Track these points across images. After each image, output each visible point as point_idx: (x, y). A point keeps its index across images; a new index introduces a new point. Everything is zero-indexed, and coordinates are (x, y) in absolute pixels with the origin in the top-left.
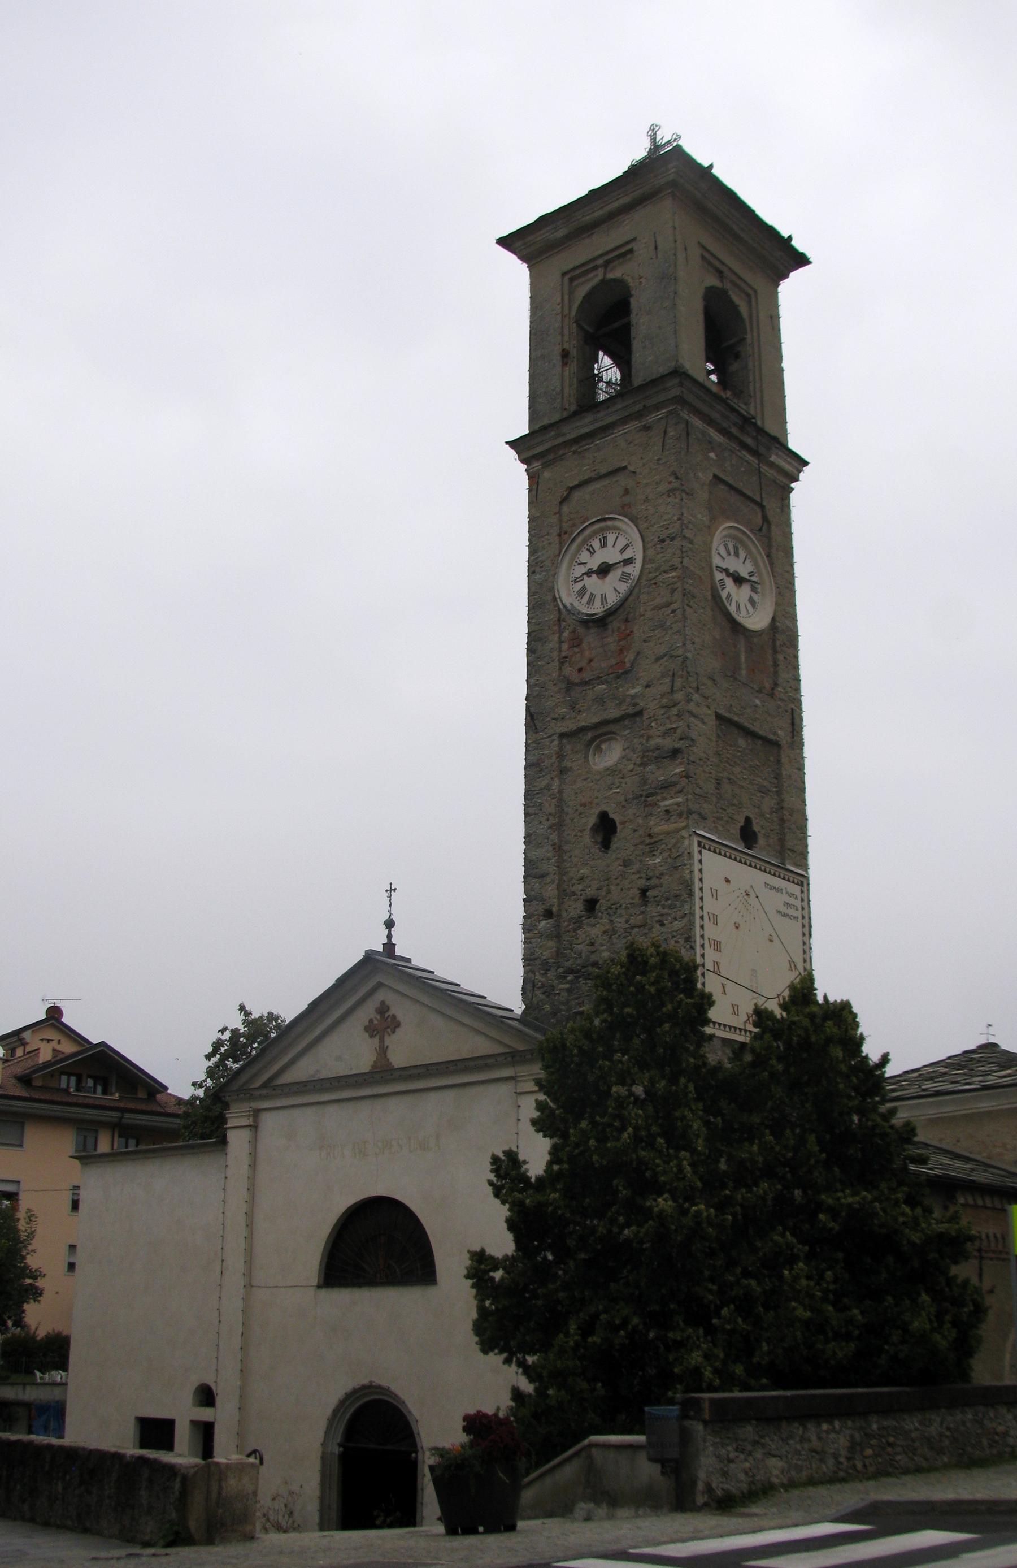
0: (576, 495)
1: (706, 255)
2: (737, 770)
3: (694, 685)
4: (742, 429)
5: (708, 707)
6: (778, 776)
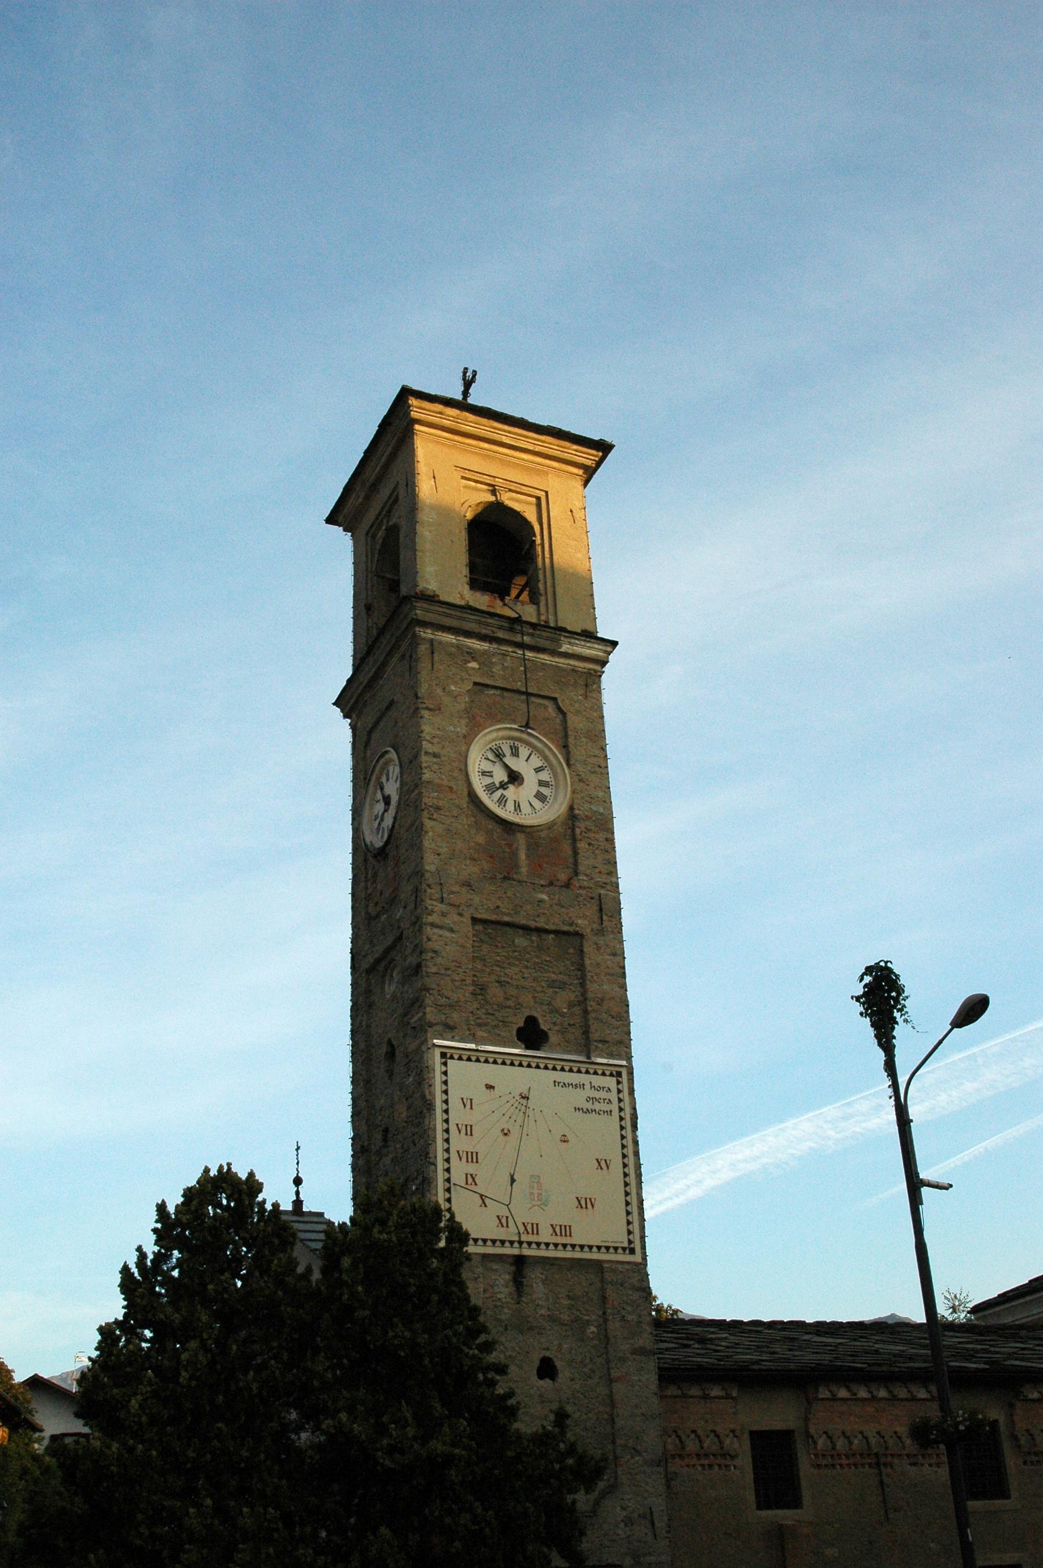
0: (375, 736)
1: (468, 475)
2: (512, 971)
3: (437, 896)
4: (511, 630)
5: (460, 915)
6: (581, 968)
